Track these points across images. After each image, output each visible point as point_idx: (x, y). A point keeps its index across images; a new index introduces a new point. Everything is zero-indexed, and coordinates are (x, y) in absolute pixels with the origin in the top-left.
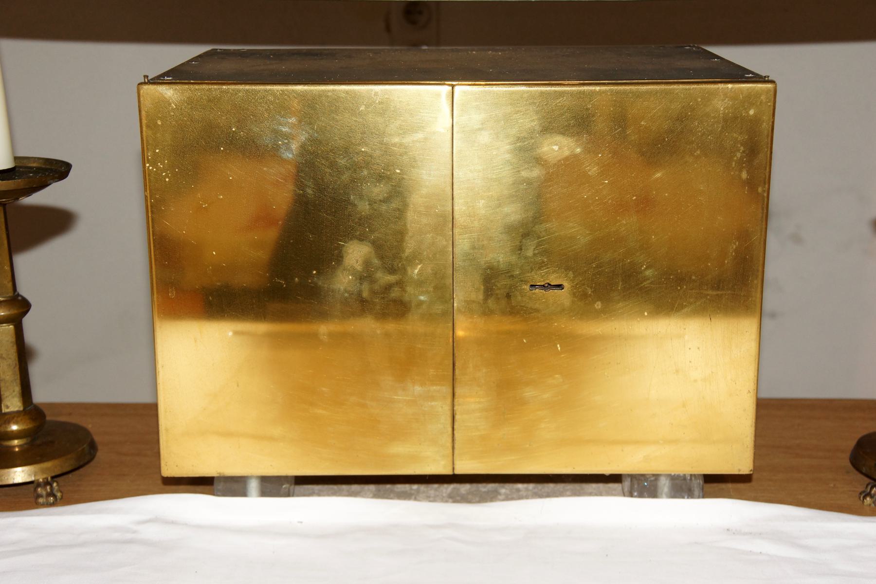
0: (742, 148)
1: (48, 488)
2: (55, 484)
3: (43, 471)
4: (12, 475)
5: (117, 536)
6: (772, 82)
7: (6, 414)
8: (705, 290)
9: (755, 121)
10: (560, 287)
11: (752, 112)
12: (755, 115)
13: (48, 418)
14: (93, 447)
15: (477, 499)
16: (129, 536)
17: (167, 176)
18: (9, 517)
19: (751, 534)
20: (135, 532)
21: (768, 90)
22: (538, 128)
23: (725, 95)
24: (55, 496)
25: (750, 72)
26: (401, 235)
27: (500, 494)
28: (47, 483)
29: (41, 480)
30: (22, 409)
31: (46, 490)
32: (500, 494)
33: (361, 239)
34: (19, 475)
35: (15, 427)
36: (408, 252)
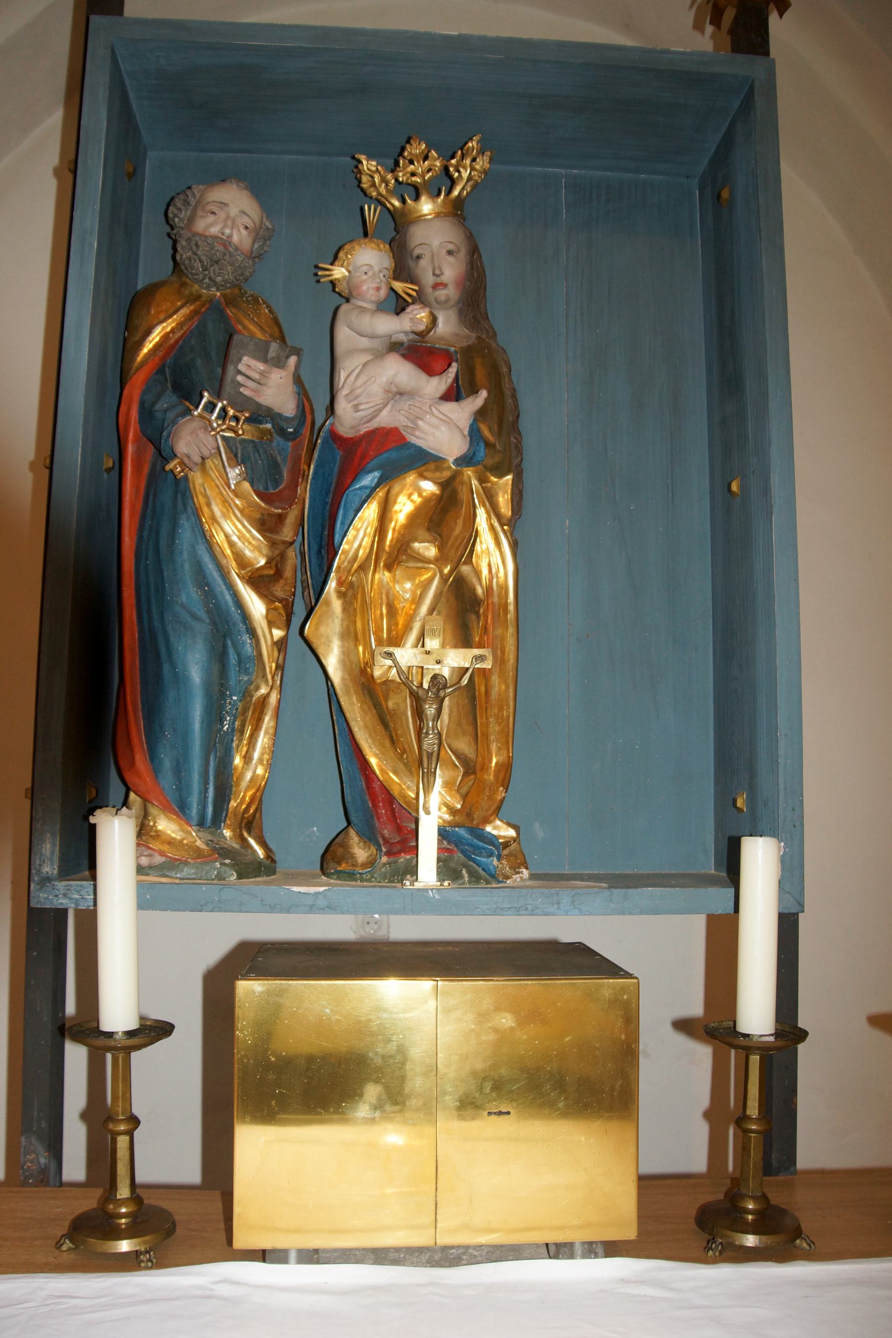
0: (621, 1020)
1: (148, 1255)
2: (152, 1253)
3: (144, 1243)
4: (117, 1246)
5: (199, 1292)
6: (637, 978)
7: (119, 1199)
8: (432, 516)
9: (628, 1003)
10: (508, 1113)
11: (625, 997)
12: (627, 998)
13: (146, 1202)
14: (174, 1224)
15: (448, 1264)
16: (208, 1293)
17: (249, 1040)
18: (123, 1276)
19: (644, 1282)
20: (212, 1290)
21: (635, 983)
22: (492, 1008)
23: (609, 987)
24: (152, 1261)
25: (622, 970)
26: (403, 1079)
27: (463, 1259)
28: (147, 1252)
29: (143, 1250)
30: (130, 1196)
31: (146, 1257)
32: (463, 1259)
33: (377, 1081)
34: (125, 1246)
35: (124, 1210)
36: (407, 1090)
